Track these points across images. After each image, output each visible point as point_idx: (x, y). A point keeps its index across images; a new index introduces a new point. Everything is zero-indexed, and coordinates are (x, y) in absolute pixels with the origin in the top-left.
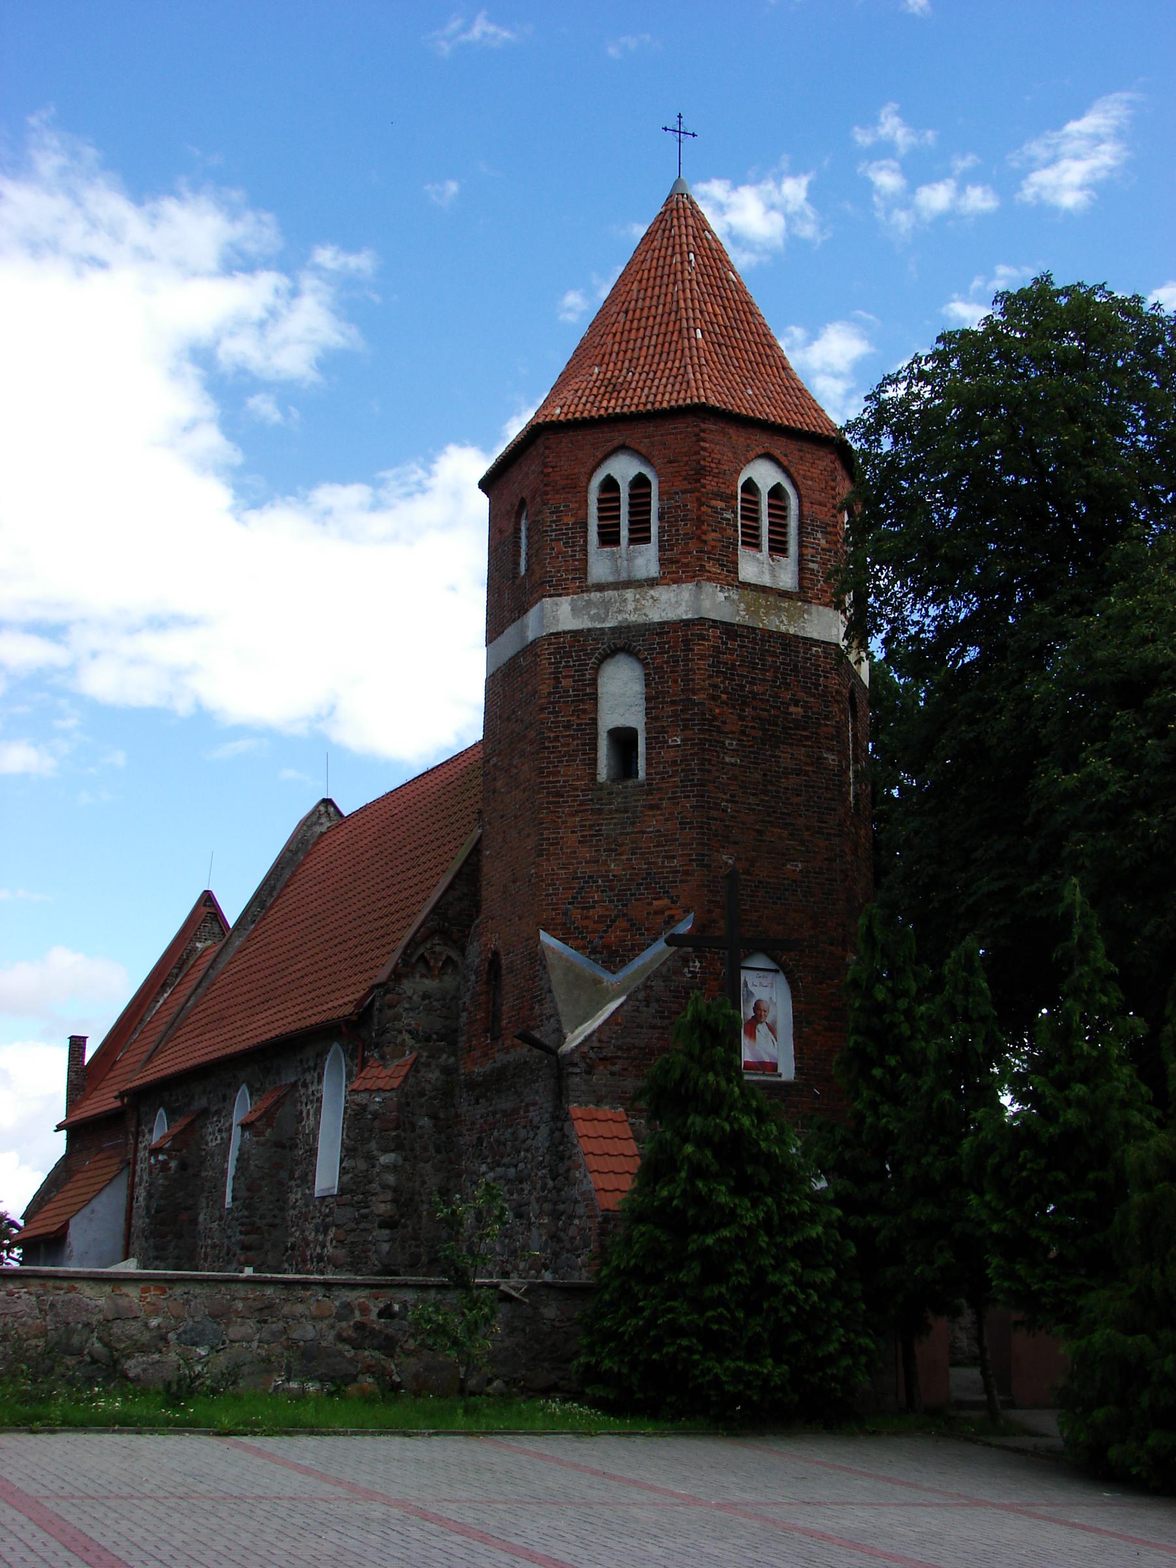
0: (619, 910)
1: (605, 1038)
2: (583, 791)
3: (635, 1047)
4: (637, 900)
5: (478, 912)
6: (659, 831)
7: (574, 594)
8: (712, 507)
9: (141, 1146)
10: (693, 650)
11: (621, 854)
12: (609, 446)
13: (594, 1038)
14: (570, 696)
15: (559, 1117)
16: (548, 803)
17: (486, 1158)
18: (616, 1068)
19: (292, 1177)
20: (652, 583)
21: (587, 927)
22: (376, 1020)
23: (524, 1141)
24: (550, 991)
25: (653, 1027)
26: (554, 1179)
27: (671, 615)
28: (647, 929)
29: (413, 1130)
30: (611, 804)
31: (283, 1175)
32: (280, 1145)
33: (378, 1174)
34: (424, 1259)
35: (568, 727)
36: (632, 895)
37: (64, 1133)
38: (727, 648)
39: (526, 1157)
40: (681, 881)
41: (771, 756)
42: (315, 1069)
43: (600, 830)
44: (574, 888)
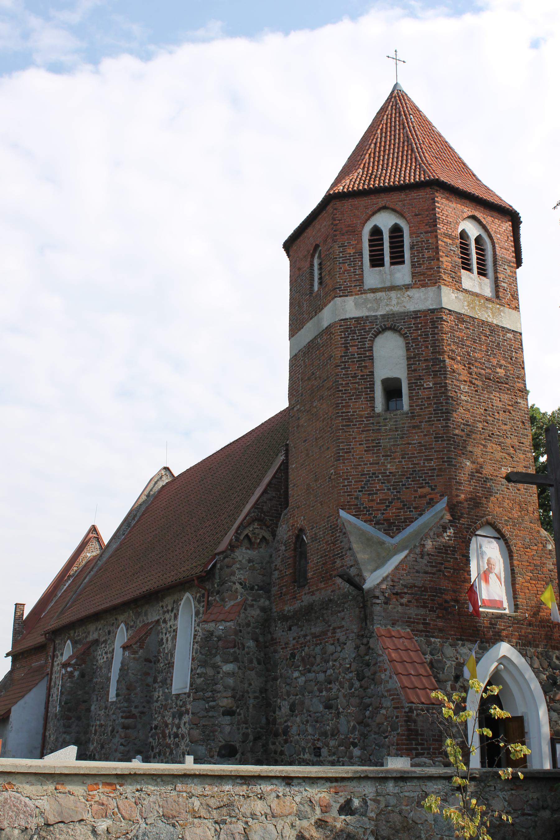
0: (395, 495)
1: (396, 580)
2: (366, 417)
3: (415, 586)
4: (407, 488)
5: (288, 506)
6: (420, 443)
7: (356, 295)
8: (445, 242)
9: (55, 664)
10: (437, 327)
11: (394, 459)
12: (376, 207)
13: (389, 579)
14: (355, 358)
15: (364, 636)
16: (342, 426)
17: (299, 667)
18: (404, 600)
19: (155, 681)
20: (407, 287)
21: (372, 507)
22: (217, 576)
23: (332, 654)
24: (350, 549)
25: (426, 573)
26: (359, 680)
27: (422, 306)
28: (414, 508)
29: (244, 649)
30: (386, 425)
31: (150, 680)
32: (148, 660)
33: (222, 678)
34: (251, 737)
35: (355, 377)
36: (403, 485)
37: (10, 658)
38: (458, 328)
39: (334, 665)
40: (437, 476)
41: (488, 398)
42: (172, 611)
43: (379, 443)
44: (363, 481)
